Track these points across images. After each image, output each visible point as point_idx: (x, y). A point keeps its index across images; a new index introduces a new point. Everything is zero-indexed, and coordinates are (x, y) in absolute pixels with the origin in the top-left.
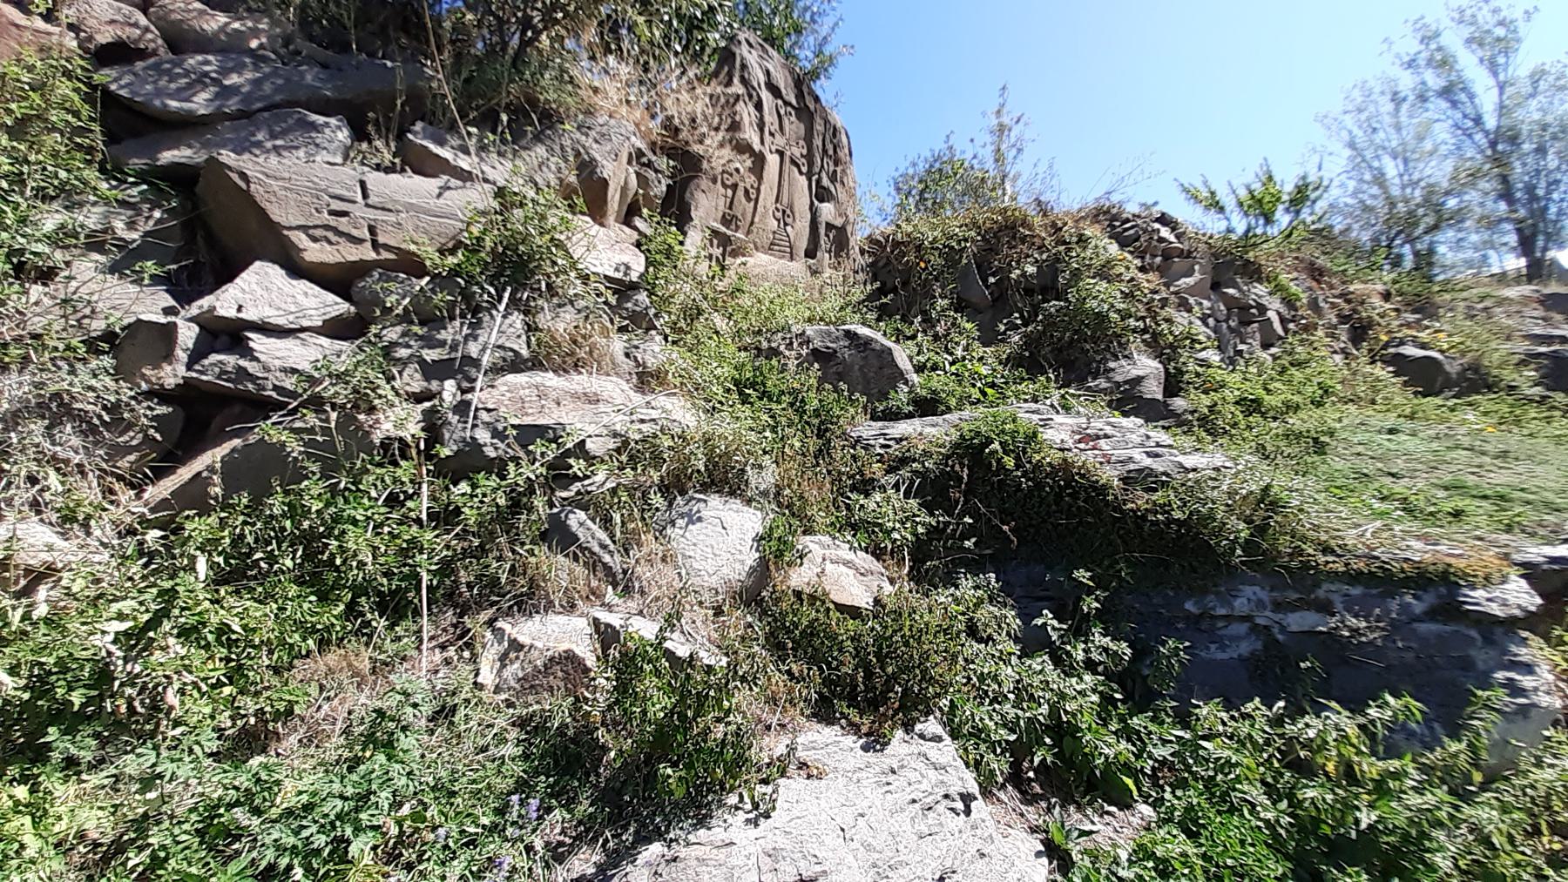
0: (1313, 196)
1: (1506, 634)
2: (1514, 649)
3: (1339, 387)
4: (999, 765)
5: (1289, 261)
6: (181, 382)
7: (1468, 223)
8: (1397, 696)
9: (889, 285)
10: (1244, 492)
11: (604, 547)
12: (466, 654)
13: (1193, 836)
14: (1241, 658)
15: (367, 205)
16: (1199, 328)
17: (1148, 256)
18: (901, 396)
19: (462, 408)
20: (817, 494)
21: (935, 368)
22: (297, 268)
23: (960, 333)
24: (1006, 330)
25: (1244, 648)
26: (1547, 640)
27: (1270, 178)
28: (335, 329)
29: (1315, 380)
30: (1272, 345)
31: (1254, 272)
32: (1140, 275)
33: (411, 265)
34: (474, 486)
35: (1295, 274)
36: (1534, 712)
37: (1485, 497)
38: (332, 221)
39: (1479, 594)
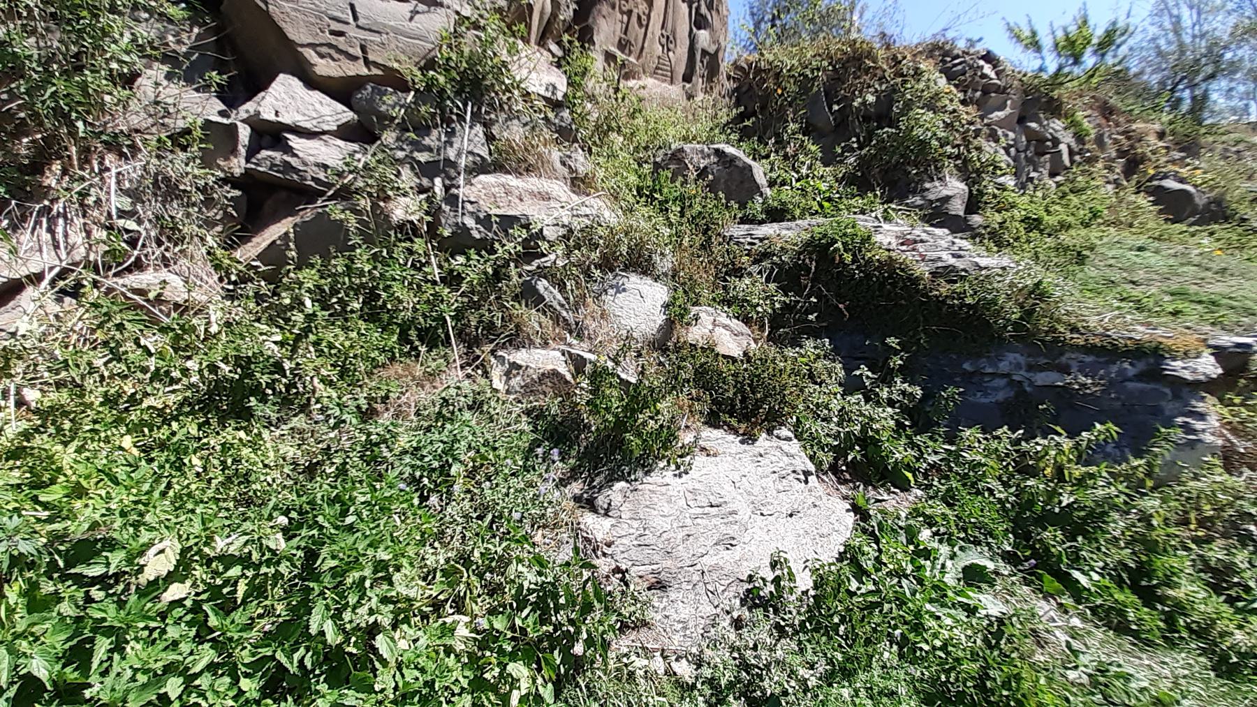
0: (1119, 41)
2: (1194, 402)
3: (1106, 212)
4: (827, 458)
7: (1238, 76)
9: (750, 109)
11: (562, 306)
12: (480, 372)
13: (950, 505)
14: (997, 403)
15: (358, 26)
16: (1002, 157)
18: (757, 205)
19: (452, 200)
20: (705, 279)
21: (783, 183)
22: (312, 82)
23: (806, 155)
25: (1001, 396)
26: (1221, 400)
27: (1085, 22)
28: (345, 133)
29: (1088, 206)
30: (1058, 174)
31: (1055, 108)
32: (961, 107)
33: (397, 82)
34: (468, 259)
35: (1089, 112)
36: (1199, 445)
38: (333, 40)
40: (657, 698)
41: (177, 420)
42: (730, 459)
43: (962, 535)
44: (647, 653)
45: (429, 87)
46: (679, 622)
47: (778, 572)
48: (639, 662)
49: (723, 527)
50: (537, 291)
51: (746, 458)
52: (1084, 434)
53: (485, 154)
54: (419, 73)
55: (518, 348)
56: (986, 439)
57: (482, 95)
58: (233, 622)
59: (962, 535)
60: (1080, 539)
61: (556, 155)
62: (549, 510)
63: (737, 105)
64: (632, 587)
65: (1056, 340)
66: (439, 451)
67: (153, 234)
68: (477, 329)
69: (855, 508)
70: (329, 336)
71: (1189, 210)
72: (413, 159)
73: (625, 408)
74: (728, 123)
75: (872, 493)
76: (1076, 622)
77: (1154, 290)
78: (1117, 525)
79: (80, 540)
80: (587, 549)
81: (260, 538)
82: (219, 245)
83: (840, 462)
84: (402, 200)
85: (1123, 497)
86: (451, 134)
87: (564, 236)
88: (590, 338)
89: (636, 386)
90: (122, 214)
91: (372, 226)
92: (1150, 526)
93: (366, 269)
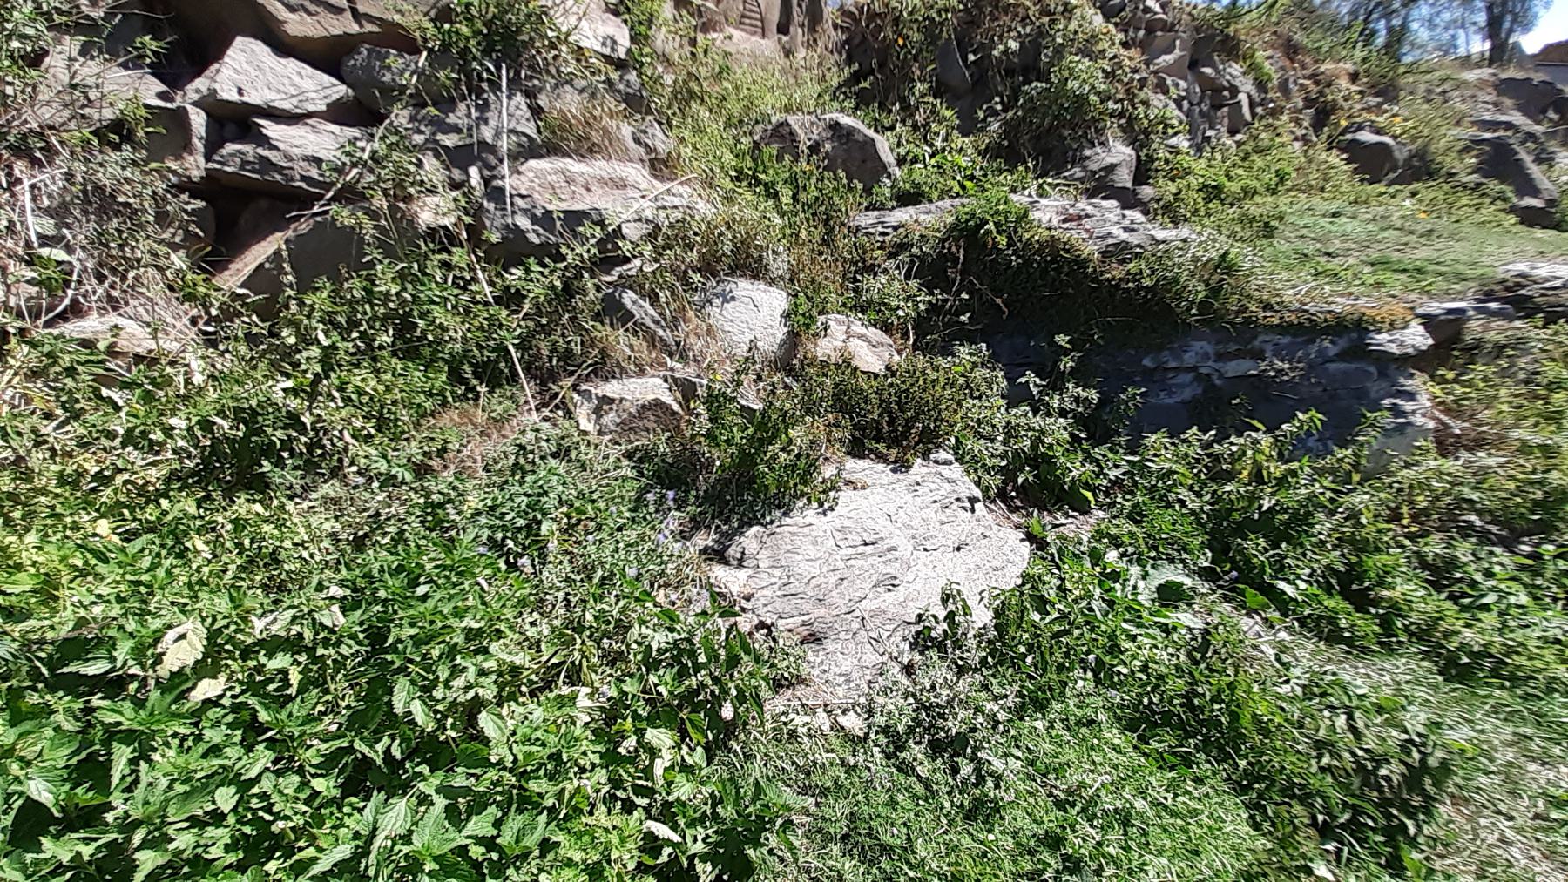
1: (1397, 369)
2: (1402, 380)
3: (1294, 175)
5: (1267, 36)
6: (204, 174)
8: (1305, 412)
10: (1205, 259)
12: (560, 413)
13: (1137, 523)
14: (1183, 403)
16: (1173, 112)
17: (1132, 29)
18: (885, 189)
19: (496, 194)
21: (915, 160)
22: (283, 46)
23: (940, 123)
24: (986, 117)
25: (1187, 394)
26: (1432, 377)
28: (338, 113)
30: (1238, 132)
31: (1231, 49)
33: (398, 39)
34: (528, 271)
35: (1269, 53)
36: (1409, 430)
37: (1405, 271)
39: (1384, 337)
40: (825, 755)
41: (167, 497)
42: (882, 490)
43: (1153, 554)
44: (807, 709)
45: (446, 47)
46: (840, 675)
47: (951, 607)
48: (799, 720)
49: (882, 567)
50: (623, 306)
51: (901, 487)
52: (1284, 427)
53: (532, 132)
54: (430, 25)
55: (606, 380)
56: (1173, 444)
57: (520, 55)
58: (290, 715)
59: (1153, 554)
60: (1284, 545)
61: (626, 130)
62: (670, 566)
63: (849, 62)
64: (781, 642)
65: (1247, 321)
66: (523, 506)
67: (90, 264)
68: (550, 360)
69: (1030, 537)
70: (357, 381)
71: (1387, 166)
72: (437, 142)
73: (751, 439)
74: (840, 86)
75: (1048, 519)
76: (1283, 635)
77: (1351, 261)
78: (1323, 526)
79: (65, 640)
80: (725, 605)
81: (310, 613)
82: (190, 269)
83: (1009, 488)
84: (431, 200)
85: (1329, 494)
86: (484, 107)
87: (650, 235)
88: (696, 361)
89: (763, 413)
90: (45, 240)
91: (394, 234)
92: (1359, 525)
93: (393, 291)
